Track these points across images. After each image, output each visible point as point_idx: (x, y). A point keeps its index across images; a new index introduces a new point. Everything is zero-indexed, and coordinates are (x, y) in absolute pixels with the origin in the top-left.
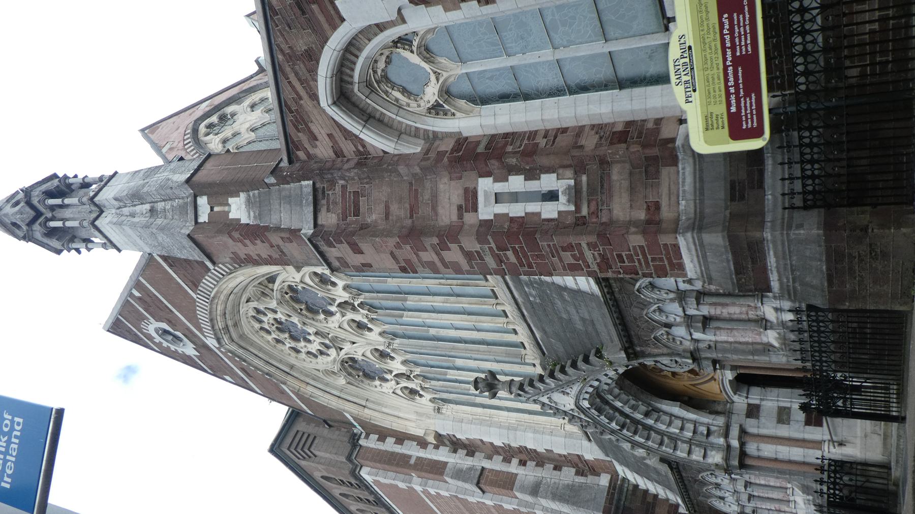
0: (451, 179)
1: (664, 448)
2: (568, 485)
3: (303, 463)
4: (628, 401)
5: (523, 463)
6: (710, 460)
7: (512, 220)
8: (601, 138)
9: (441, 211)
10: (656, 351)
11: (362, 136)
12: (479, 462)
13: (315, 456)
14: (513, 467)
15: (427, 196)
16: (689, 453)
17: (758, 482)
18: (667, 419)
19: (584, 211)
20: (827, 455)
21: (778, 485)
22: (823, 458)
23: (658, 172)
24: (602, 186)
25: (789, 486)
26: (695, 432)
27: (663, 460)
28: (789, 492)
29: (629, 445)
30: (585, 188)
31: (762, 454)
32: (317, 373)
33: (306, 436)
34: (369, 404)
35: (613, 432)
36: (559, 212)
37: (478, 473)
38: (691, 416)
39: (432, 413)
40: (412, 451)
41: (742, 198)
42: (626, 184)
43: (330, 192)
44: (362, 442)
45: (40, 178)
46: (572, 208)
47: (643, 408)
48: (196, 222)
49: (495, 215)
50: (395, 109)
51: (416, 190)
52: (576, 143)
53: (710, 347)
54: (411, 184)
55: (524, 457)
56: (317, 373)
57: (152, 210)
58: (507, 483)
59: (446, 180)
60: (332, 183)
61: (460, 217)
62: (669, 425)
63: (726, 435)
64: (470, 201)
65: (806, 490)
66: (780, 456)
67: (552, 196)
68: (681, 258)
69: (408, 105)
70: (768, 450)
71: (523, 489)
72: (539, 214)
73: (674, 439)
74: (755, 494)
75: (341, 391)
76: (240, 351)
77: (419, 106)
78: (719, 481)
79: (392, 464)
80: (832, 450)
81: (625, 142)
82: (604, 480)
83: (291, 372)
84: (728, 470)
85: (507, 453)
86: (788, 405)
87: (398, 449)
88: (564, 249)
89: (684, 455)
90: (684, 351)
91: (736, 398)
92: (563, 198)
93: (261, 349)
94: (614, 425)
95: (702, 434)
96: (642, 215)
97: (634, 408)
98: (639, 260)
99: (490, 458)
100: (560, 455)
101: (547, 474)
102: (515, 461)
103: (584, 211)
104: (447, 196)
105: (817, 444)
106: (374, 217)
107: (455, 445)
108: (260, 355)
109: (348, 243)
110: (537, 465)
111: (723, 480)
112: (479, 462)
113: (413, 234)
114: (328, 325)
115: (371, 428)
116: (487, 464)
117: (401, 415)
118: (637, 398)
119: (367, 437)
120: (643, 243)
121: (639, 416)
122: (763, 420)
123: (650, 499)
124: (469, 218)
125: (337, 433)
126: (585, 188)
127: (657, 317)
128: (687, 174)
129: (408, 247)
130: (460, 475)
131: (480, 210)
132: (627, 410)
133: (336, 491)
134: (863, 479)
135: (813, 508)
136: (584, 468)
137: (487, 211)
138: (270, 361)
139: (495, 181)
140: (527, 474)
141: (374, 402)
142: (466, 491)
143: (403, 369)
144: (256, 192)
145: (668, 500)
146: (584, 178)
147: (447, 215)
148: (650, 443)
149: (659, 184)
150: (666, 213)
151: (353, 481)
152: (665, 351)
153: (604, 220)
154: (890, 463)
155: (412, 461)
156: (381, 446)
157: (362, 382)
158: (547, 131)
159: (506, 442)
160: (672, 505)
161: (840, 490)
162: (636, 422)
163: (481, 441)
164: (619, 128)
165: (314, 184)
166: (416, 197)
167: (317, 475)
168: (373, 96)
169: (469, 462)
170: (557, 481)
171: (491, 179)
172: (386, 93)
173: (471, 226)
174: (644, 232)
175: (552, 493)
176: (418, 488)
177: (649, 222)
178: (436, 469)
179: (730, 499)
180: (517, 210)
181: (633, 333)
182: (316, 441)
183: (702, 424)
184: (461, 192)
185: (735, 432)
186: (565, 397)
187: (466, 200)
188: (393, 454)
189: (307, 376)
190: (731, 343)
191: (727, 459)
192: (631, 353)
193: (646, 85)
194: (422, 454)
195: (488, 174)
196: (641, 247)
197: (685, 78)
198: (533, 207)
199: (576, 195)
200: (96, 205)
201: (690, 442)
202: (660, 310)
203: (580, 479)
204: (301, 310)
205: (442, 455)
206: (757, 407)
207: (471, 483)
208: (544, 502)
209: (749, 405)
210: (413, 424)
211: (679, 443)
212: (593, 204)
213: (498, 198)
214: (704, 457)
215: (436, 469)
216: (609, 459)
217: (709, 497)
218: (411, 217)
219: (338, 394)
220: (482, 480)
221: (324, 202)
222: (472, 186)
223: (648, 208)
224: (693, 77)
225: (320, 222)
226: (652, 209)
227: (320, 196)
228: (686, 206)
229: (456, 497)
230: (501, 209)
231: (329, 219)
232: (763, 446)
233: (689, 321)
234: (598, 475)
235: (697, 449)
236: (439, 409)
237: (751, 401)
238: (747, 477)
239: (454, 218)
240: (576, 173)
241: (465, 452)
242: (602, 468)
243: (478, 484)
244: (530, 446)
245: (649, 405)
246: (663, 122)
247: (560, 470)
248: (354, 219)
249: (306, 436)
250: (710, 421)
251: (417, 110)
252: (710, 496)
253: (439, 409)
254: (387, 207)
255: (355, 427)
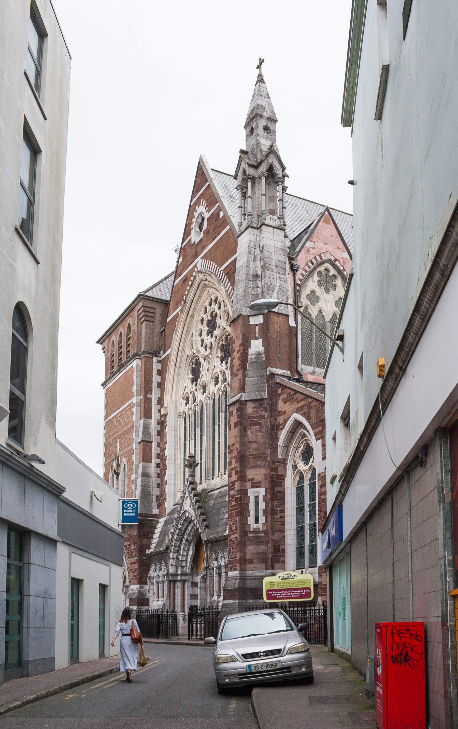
0: (265, 475)
1: (173, 548)
2: (150, 493)
3: (135, 313)
4: (192, 532)
5: (158, 465)
6: (170, 567)
7: (247, 504)
8: (278, 541)
9: (252, 470)
10: (208, 552)
11: (284, 430)
12: (154, 439)
13: (142, 323)
14: (155, 460)
15: (259, 463)
16: (173, 559)
17: (165, 586)
18: (186, 549)
19: (250, 535)
20: (178, 614)
21: (165, 594)
22: (177, 612)
23: (263, 563)
24: (259, 542)
25: (165, 599)
26: (182, 561)
27: (168, 547)
28: (162, 599)
29: (173, 532)
30: (259, 535)
31: (176, 588)
32: (190, 334)
33: (151, 315)
34: (177, 368)
35: (177, 525)
36: (250, 525)
37: (149, 440)
38: (189, 559)
39: (178, 412)
40: (155, 396)
41: (251, 592)
42: (260, 551)
43: (262, 409)
44: (155, 359)
45: (283, 161)
46: (251, 530)
47: (189, 539)
48: (249, 316)
49: (249, 496)
50: (296, 446)
51: (261, 457)
52: (276, 531)
53: (211, 574)
54: (264, 454)
55: (161, 465)
56: (190, 334)
57: (257, 276)
58: (146, 458)
59: (265, 472)
60: (265, 410)
61: (249, 480)
62: (183, 555)
63: (182, 574)
64: (256, 485)
65: (164, 605)
66: (176, 596)
67: (257, 520)
68: (234, 571)
69: (298, 452)
70: (178, 591)
71: (144, 468)
72: (249, 516)
73: (178, 552)
74: (160, 585)
75: (183, 350)
76: (196, 284)
77: (297, 458)
78: (163, 570)
79: (145, 383)
80: (181, 616)
81: (274, 551)
82: (156, 511)
83: (189, 317)
84: (168, 574)
85: (161, 456)
86: (199, 598)
87: (154, 385)
88: (236, 527)
89: (170, 563)
90: (209, 564)
91: (200, 577)
92: (256, 526)
93: (200, 296)
94: (180, 526)
95: (182, 564)
96: (248, 557)
97: (189, 535)
98: (232, 555)
99: (158, 445)
100: (165, 488)
101: (154, 480)
102: (158, 461)
103: (250, 535)
104: (258, 473)
105: (183, 610)
106: (250, 435)
107: (162, 423)
108: (196, 297)
109: (237, 422)
110: (158, 474)
111: (164, 571)
112: (154, 439)
113: (242, 458)
114: (215, 358)
115: (164, 363)
116: (154, 445)
117: (174, 390)
118: (193, 536)
119: (159, 362)
120: (237, 558)
121: (186, 537)
122: (191, 589)
123: (150, 535)
124: (249, 484)
125: (158, 339)
126: (259, 535)
127: (220, 555)
128: (262, 573)
129: (236, 454)
130: (146, 428)
131: (252, 489)
132: (188, 532)
133: (122, 329)
134: (171, 627)
135: (158, 608)
136: (161, 500)
137: (251, 492)
138: (193, 303)
139: (264, 496)
140: (153, 469)
141: (179, 371)
142: (137, 432)
143: (198, 400)
144: (264, 359)
145: (151, 544)
146: (263, 535)
147: (251, 473)
148: (174, 542)
149: (259, 563)
150: (248, 566)
151: (130, 354)
152: (209, 556)
153: (247, 543)
154: (178, 636)
155: (149, 396)
156: (154, 373)
157: (190, 366)
158: (284, 517)
159: (167, 458)
160: (149, 546)
161: (165, 619)
162: (183, 535)
163: (166, 443)
164: (282, 547)
165: (266, 399)
166: (258, 457)
167: (129, 320)
168: (301, 437)
169: (154, 433)
170: (151, 486)
171: (264, 494)
172: (302, 443)
173: (245, 486)
174: (241, 559)
175: (145, 484)
176: (134, 400)
177: (245, 560)
178: (147, 414)
179: (156, 574)
180: (251, 506)
181: (214, 544)
182: (151, 324)
183: (186, 564)
184: (260, 480)
185: (184, 578)
186: (189, 506)
187: (256, 483)
188: (152, 381)
189: (188, 326)
190: (213, 582)
191: (172, 575)
192: (208, 541)
193: (297, 557)
194: (154, 402)
195: (266, 493)
196: (236, 557)
197: (285, 576)
198: (252, 513)
199: (257, 531)
200: (261, 226)
201: (177, 558)
202: (222, 557)
203: (154, 498)
204: (222, 341)
205: (155, 416)
206: (197, 586)
207: (143, 437)
208: (139, 480)
209: (197, 583)
210: (169, 398)
211: (176, 554)
212: (253, 538)
213: (257, 497)
214: (172, 565)
215: (147, 414)
216: (166, 515)
217: (155, 565)
218: (250, 455)
219: (180, 348)
220: (146, 443)
221: (258, 405)
222: (262, 485)
223: (250, 559)
224: (285, 579)
225: (248, 403)
226: (250, 561)
227: (261, 402)
228: (250, 573)
229: (133, 426)
230: (252, 499)
231: (249, 409)
232: (180, 589)
233: (219, 568)
234: (158, 508)
235: (175, 562)
236: (180, 415)
237: (199, 583)
238: (166, 582)
239: (249, 477)
240: (265, 531)
241: (159, 430)
242: (161, 510)
243: (143, 441)
244: (167, 471)
245: (191, 541)
246: (283, 564)
247: (158, 487)
248: (249, 423)
249: (151, 315)
250: (188, 567)
251: (296, 457)
252: (156, 566)
253: (180, 415)
254: (254, 442)
255: (164, 353)
